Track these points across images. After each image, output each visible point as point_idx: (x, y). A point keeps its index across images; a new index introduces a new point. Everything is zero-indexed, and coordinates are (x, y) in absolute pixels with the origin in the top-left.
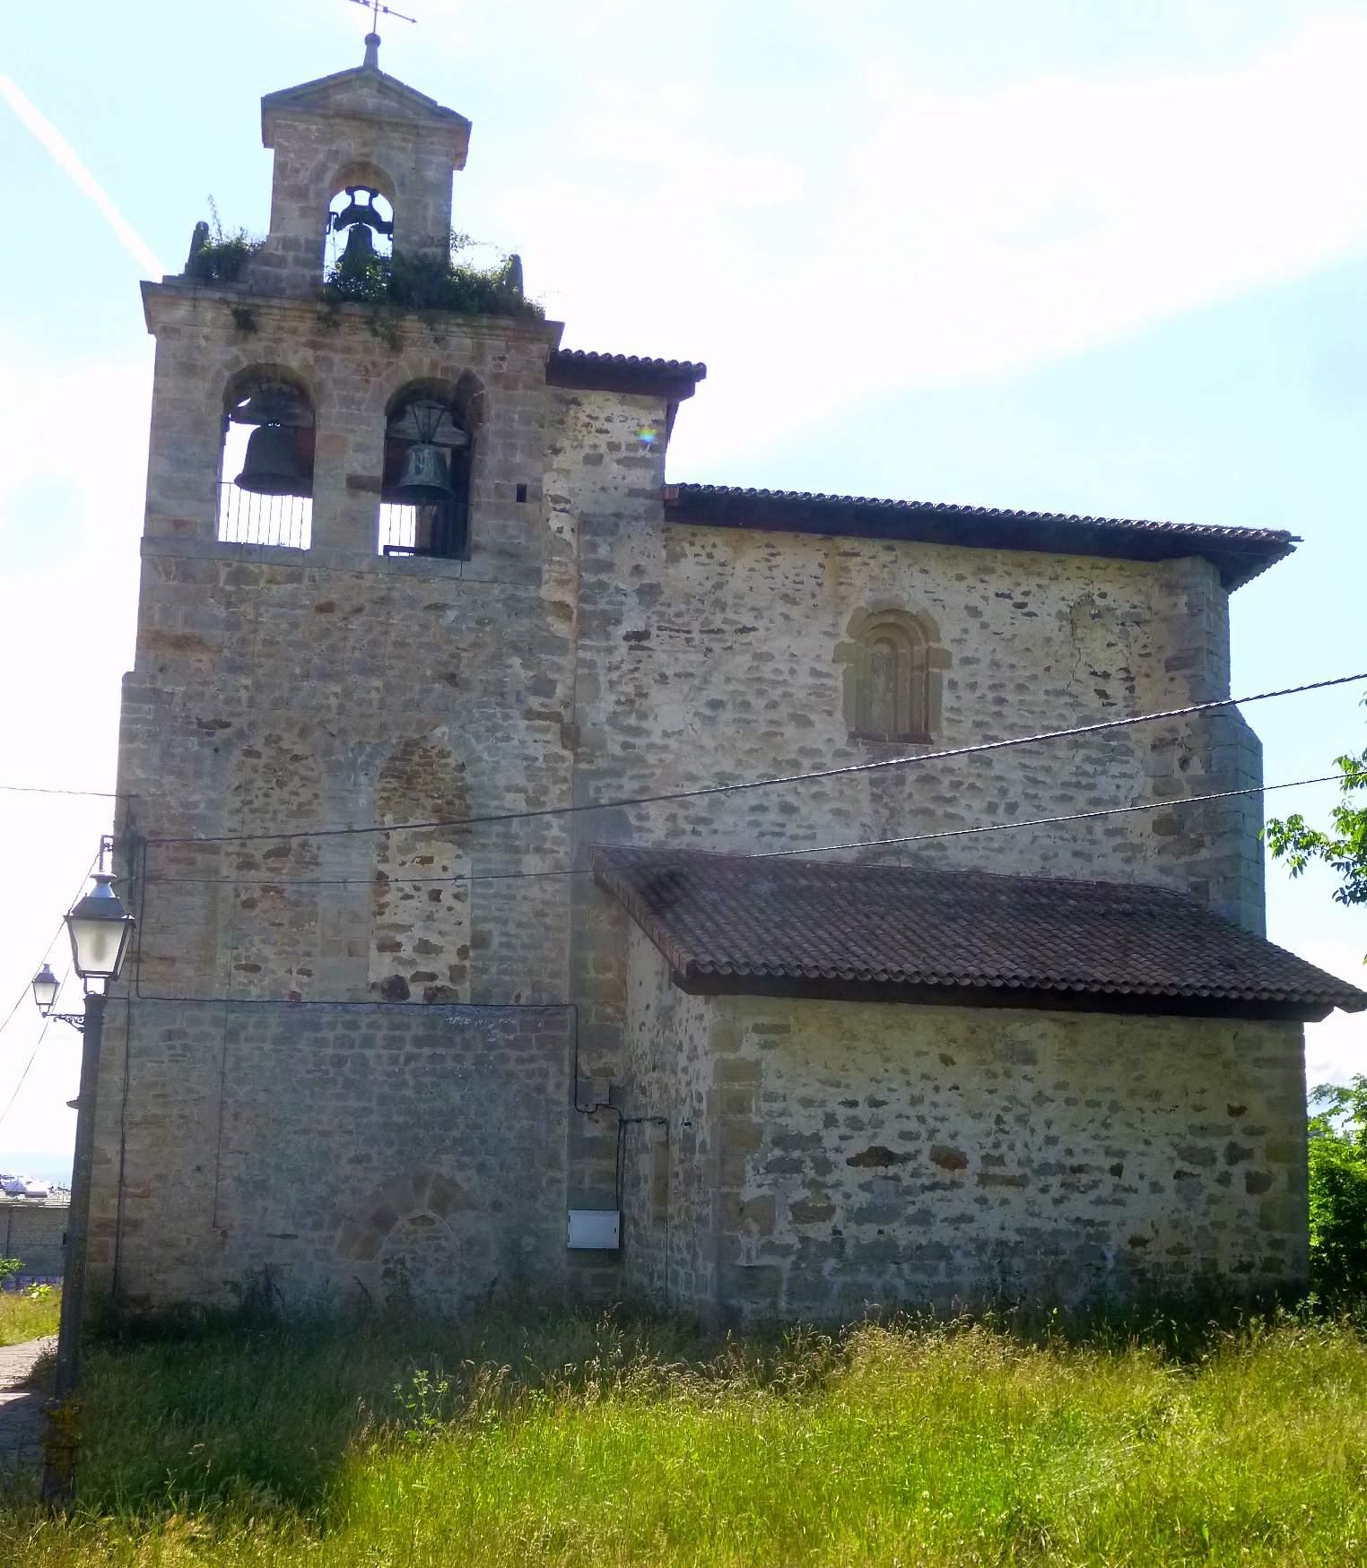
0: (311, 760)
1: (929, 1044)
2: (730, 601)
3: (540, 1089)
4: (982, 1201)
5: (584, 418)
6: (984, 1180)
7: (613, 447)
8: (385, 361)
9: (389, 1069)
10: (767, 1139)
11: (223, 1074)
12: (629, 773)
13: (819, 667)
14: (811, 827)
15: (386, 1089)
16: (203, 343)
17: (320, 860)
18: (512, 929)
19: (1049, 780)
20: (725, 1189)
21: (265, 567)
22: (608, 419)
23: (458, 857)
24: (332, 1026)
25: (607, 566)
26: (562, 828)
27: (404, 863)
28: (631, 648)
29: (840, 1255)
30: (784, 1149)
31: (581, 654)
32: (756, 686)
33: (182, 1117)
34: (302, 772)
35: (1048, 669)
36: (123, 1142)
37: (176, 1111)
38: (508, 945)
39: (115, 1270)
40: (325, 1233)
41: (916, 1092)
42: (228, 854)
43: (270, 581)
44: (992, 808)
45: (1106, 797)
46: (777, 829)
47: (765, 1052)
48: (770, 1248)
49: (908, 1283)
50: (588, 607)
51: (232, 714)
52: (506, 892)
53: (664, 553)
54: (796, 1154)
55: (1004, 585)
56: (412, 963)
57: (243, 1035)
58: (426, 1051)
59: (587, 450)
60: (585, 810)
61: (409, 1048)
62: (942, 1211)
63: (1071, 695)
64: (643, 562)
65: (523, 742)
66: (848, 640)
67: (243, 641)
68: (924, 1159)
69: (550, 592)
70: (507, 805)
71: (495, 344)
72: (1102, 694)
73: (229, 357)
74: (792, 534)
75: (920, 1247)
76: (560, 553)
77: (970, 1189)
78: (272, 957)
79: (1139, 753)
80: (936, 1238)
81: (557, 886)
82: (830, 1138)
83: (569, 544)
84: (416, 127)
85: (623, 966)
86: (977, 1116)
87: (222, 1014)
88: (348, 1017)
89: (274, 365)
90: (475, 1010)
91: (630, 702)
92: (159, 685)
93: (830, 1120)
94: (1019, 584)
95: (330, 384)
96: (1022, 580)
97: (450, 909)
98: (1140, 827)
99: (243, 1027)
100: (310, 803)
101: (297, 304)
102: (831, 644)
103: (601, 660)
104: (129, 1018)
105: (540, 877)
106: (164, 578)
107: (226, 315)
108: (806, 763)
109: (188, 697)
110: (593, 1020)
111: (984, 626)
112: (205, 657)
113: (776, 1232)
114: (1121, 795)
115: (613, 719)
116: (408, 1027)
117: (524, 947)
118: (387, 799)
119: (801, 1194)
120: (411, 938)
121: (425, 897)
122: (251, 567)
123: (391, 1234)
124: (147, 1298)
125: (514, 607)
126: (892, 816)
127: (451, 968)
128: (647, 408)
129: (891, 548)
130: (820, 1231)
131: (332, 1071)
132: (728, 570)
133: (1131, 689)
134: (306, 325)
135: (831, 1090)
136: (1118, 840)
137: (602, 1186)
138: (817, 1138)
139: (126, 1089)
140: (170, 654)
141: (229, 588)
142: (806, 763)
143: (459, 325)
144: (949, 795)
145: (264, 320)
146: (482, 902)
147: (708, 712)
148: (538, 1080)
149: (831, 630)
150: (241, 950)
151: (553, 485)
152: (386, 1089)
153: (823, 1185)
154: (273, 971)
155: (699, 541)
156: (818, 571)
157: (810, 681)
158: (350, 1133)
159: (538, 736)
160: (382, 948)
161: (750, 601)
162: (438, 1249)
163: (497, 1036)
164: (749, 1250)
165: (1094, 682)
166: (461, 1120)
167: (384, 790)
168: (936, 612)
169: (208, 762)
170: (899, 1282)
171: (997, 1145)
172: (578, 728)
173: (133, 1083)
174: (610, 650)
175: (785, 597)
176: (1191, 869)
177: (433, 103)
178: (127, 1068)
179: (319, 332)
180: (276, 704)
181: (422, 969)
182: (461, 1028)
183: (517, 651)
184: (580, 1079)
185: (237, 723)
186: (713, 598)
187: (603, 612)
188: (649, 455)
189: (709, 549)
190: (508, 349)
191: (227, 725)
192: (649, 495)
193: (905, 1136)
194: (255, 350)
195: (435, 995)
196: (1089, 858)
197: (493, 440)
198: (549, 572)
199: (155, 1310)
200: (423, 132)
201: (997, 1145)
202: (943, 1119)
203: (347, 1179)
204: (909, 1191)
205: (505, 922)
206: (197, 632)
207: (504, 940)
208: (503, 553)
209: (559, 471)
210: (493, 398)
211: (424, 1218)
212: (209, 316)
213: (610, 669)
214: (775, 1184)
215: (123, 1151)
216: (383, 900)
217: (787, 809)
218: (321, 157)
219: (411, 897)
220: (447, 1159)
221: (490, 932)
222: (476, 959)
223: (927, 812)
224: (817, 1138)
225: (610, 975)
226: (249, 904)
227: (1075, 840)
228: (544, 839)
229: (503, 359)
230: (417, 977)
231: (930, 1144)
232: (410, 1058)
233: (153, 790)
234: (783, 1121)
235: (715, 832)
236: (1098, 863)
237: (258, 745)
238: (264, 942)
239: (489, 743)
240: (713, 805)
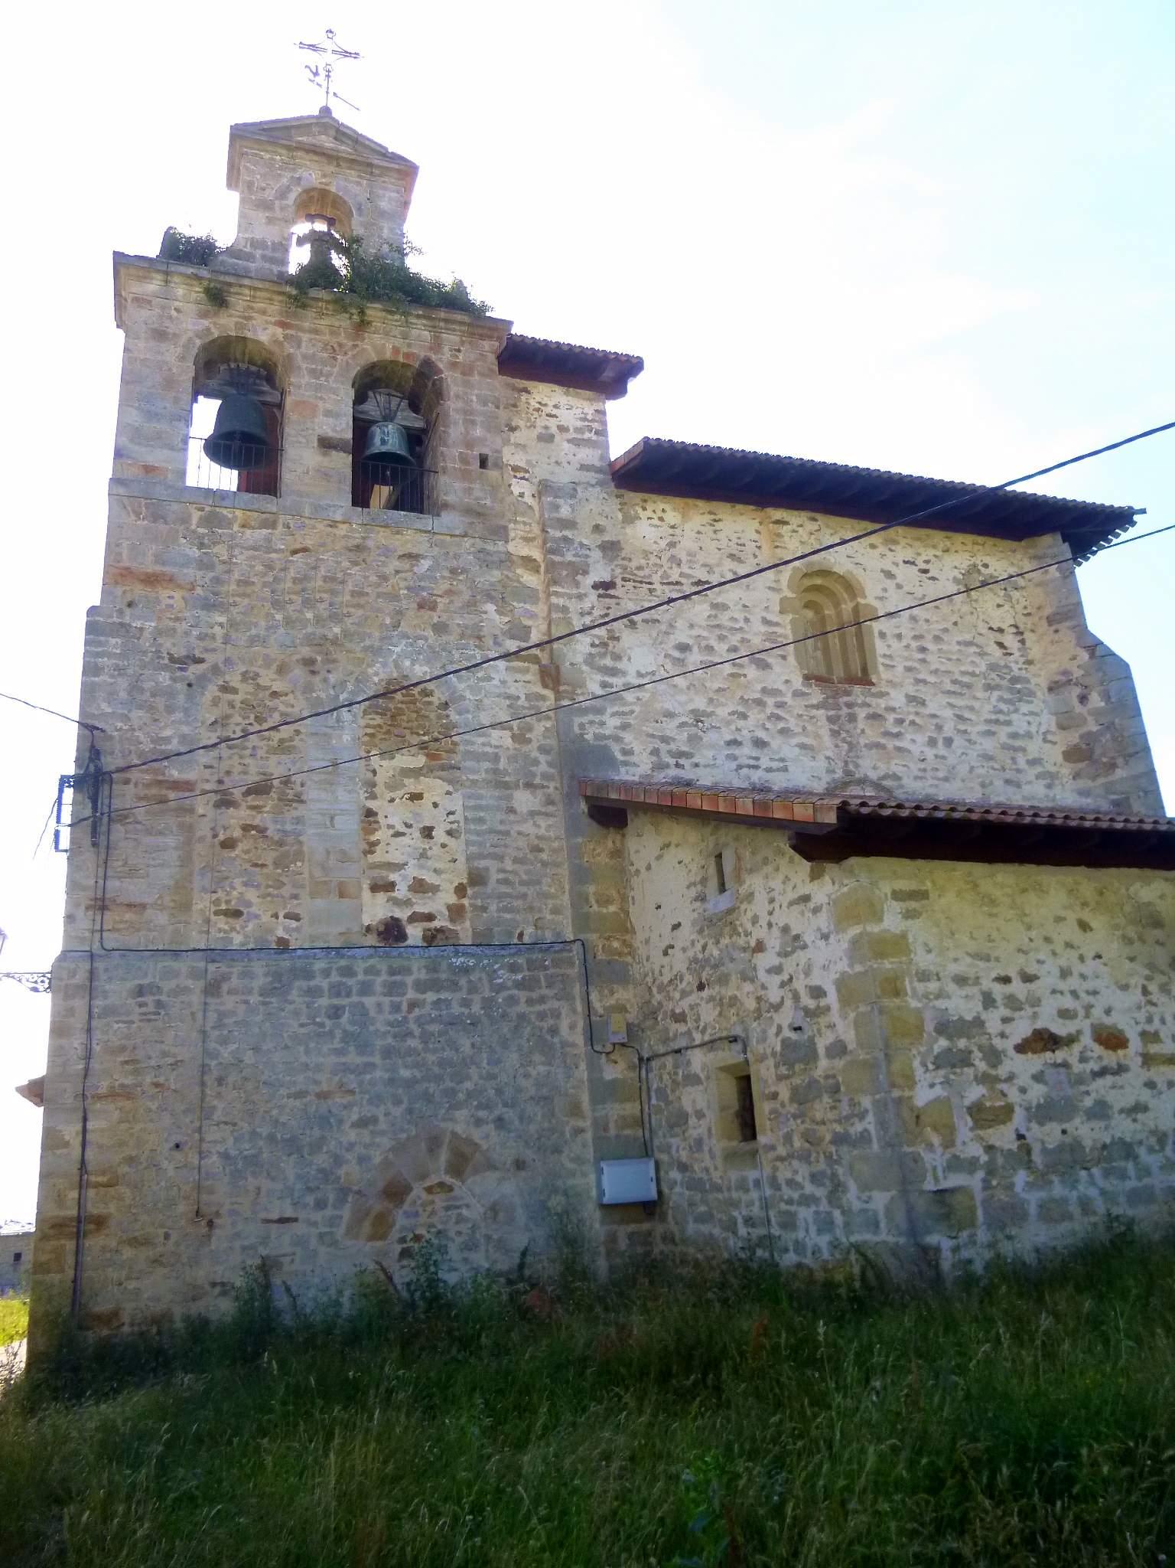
0: (291, 696)
1: (1065, 908)
2: (684, 558)
3: (554, 1031)
4: (1150, 1085)
5: (534, 404)
6: (1148, 1060)
7: (562, 429)
8: (350, 343)
9: (391, 1018)
10: (930, 1026)
11: (204, 1032)
12: (609, 711)
13: (770, 617)
14: (782, 760)
15: (390, 1040)
16: (174, 313)
17: (304, 797)
18: (509, 865)
19: (973, 717)
20: (896, 1093)
21: (238, 513)
22: (556, 406)
23: (448, 793)
24: (326, 973)
25: (570, 524)
26: (550, 764)
27: (392, 800)
28: (600, 596)
29: (1029, 1165)
30: (950, 1038)
31: (554, 600)
32: (718, 632)
33: (157, 1085)
34: (282, 708)
35: (955, 624)
37: (148, 1079)
38: (506, 882)
39: (74, 1281)
40: (329, 1212)
41: (1063, 962)
42: (204, 793)
43: (243, 526)
44: (932, 742)
45: (1022, 732)
46: (752, 762)
47: (910, 922)
48: (956, 1164)
49: (1103, 1192)
50: (557, 559)
51: (207, 650)
52: (502, 828)
53: (620, 516)
54: (962, 1043)
55: (909, 554)
56: (407, 903)
57: (225, 987)
58: (431, 996)
59: (539, 430)
61: (411, 994)
62: (1119, 1100)
63: (977, 646)
64: (602, 522)
65: (503, 682)
66: (790, 595)
67: (217, 580)
68: (1087, 1040)
69: (518, 548)
70: (493, 742)
71: (451, 338)
72: (1001, 645)
73: (200, 328)
74: (729, 505)
75: (1104, 1147)
76: (523, 514)
77: (1137, 1075)
78: (255, 900)
79: (1039, 694)
80: (1118, 1135)
81: (551, 821)
82: (993, 1021)
83: (530, 507)
84: (370, 165)
85: (624, 898)
86: (1125, 987)
87: (202, 964)
88: (343, 963)
89: (245, 339)
90: (478, 950)
91: (605, 645)
92: (127, 620)
93: (988, 1001)
94: (919, 554)
95: (299, 358)
96: (921, 550)
97: (444, 846)
98: (1053, 756)
99: (225, 978)
100: (291, 739)
101: (267, 285)
102: (776, 598)
103: (574, 606)
104: (92, 974)
105: (532, 814)
106: (133, 517)
107: (197, 292)
108: (770, 701)
109: (159, 632)
110: (601, 956)
111: (899, 586)
112: (178, 595)
113: (958, 1142)
114: (1033, 729)
115: (590, 660)
116: (408, 971)
117: (522, 883)
118: (372, 735)
119: (975, 1093)
120: (404, 877)
121: (417, 834)
122: (225, 512)
123: (406, 1207)
124: (115, 1314)
125: (486, 560)
126: (850, 750)
127: (449, 908)
128: (589, 399)
129: (814, 520)
130: (1003, 1137)
131: (328, 1023)
132: (678, 531)
133: (1023, 642)
134: (275, 308)
135: (982, 964)
136: (1039, 769)
137: (627, 1132)
138: (979, 1023)
139: (88, 1056)
140: (139, 591)
141: (201, 530)
142: (770, 701)
143: (418, 317)
144: (895, 730)
145: (232, 299)
146: (474, 838)
147: (676, 654)
148: (551, 1022)
149: (773, 585)
150: (220, 894)
151: (512, 457)
152: (390, 1040)
153: (997, 1079)
154: (257, 917)
155: (650, 506)
156: (755, 536)
157: (763, 629)
158: (352, 1092)
159: (519, 676)
160: (375, 888)
161: (701, 558)
162: (460, 1220)
163: (504, 976)
164: (935, 1168)
165: (992, 636)
166: (473, 1071)
167: (368, 726)
168: (858, 572)
169: (181, 698)
170: (1093, 1192)
171: (1150, 1020)
172: (557, 668)
173: (97, 1048)
174: (580, 597)
175: (732, 556)
176: (1109, 788)
177: (386, 149)
178: (89, 1030)
179: (288, 315)
180: (253, 641)
181: (420, 909)
182: (466, 970)
183: (490, 598)
184: (593, 1018)
185: (211, 658)
186: (669, 554)
187: (570, 563)
188: (594, 438)
189: (660, 514)
190: (463, 343)
191: (201, 661)
192: (599, 470)
193: (1065, 1014)
194: (226, 324)
195: (434, 937)
196: (1018, 786)
197: (454, 416)
198: (515, 531)
199: (126, 1329)
200: (376, 171)
201: (1150, 1020)
202: (1095, 993)
203: (351, 1146)
204: (1080, 1080)
205: (500, 858)
206: (167, 569)
207: (501, 876)
208: (468, 511)
209: (517, 445)
210: (452, 382)
211: (441, 1185)
212: (180, 291)
213: (582, 614)
214: (947, 1082)
215: (84, 1130)
216: (373, 838)
217: (760, 744)
218: (285, 180)
219: (403, 834)
220: (462, 1114)
221: (487, 869)
222: (475, 897)
223: (878, 746)
224: (979, 1023)
225: (612, 908)
226: (228, 844)
227: (1004, 770)
228: (534, 775)
229: (459, 351)
230: (414, 918)
231: (1088, 1022)
232: (412, 1005)
233: (119, 725)
234: (941, 1004)
235: (697, 765)
236: (1027, 789)
237: (234, 680)
238: (245, 884)
239: (471, 682)
240: (693, 739)
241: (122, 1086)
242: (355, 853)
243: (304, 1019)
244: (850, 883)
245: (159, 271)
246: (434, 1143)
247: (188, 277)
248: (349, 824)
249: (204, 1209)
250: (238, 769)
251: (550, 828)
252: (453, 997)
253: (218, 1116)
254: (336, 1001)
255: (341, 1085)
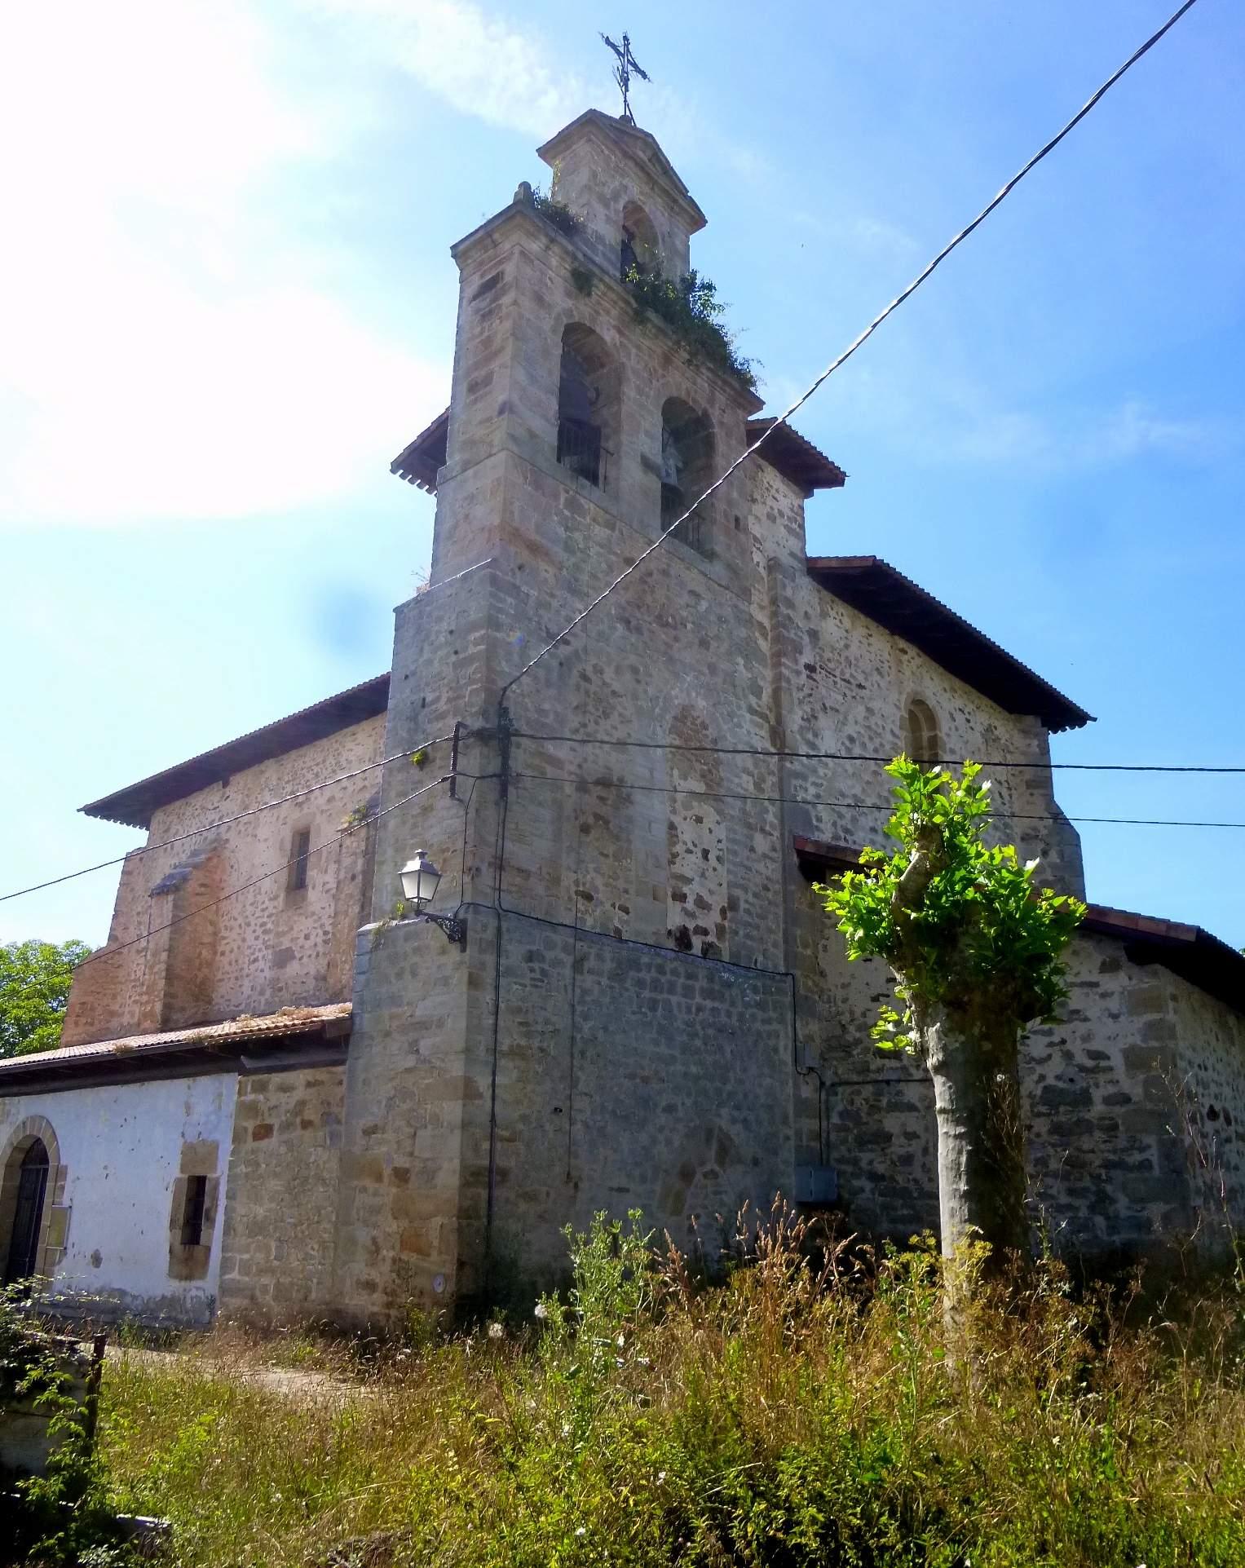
33: (542, 1050)
36: (494, 1074)
60: (786, 802)
78: (601, 888)
84: (675, 201)
88: (659, 961)
104: (499, 929)
122: (583, 501)
143: (709, 369)
152: (685, 1038)
178: (497, 988)
182: (729, 985)
212: (554, 262)
241: (518, 1045)
242: (664, 862)
243: (635, 1008)
244: (1154, 982)
245: (547, 235)
246: (709, 1133)
247: (567, 252)
248: (660, 831)
249: (574, 1173)
250: (591, 758)
251: (771, 870)
252: (723, 1007)
253: (581, 1087)
254: (653, 995)
255: (657, 1072)
